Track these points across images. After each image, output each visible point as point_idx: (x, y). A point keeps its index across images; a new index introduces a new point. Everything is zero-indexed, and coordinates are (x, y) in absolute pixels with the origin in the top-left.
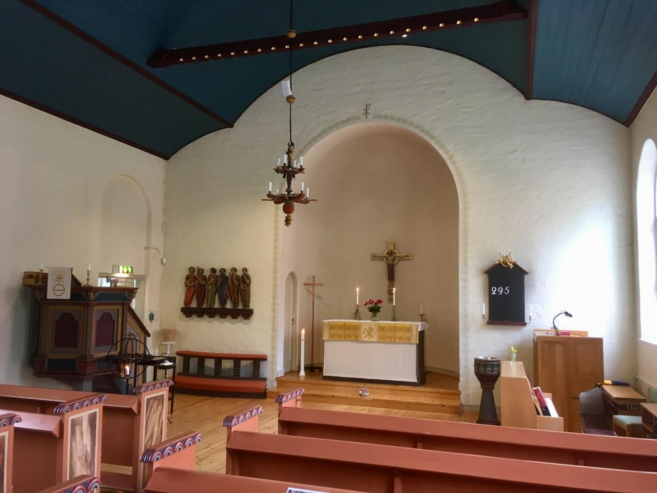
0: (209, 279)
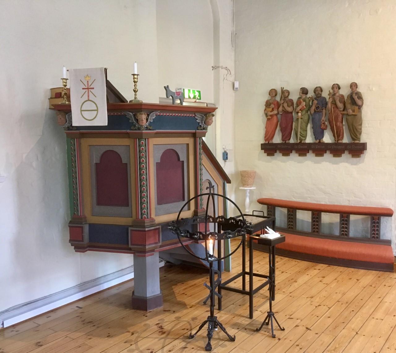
0: (299, 103)
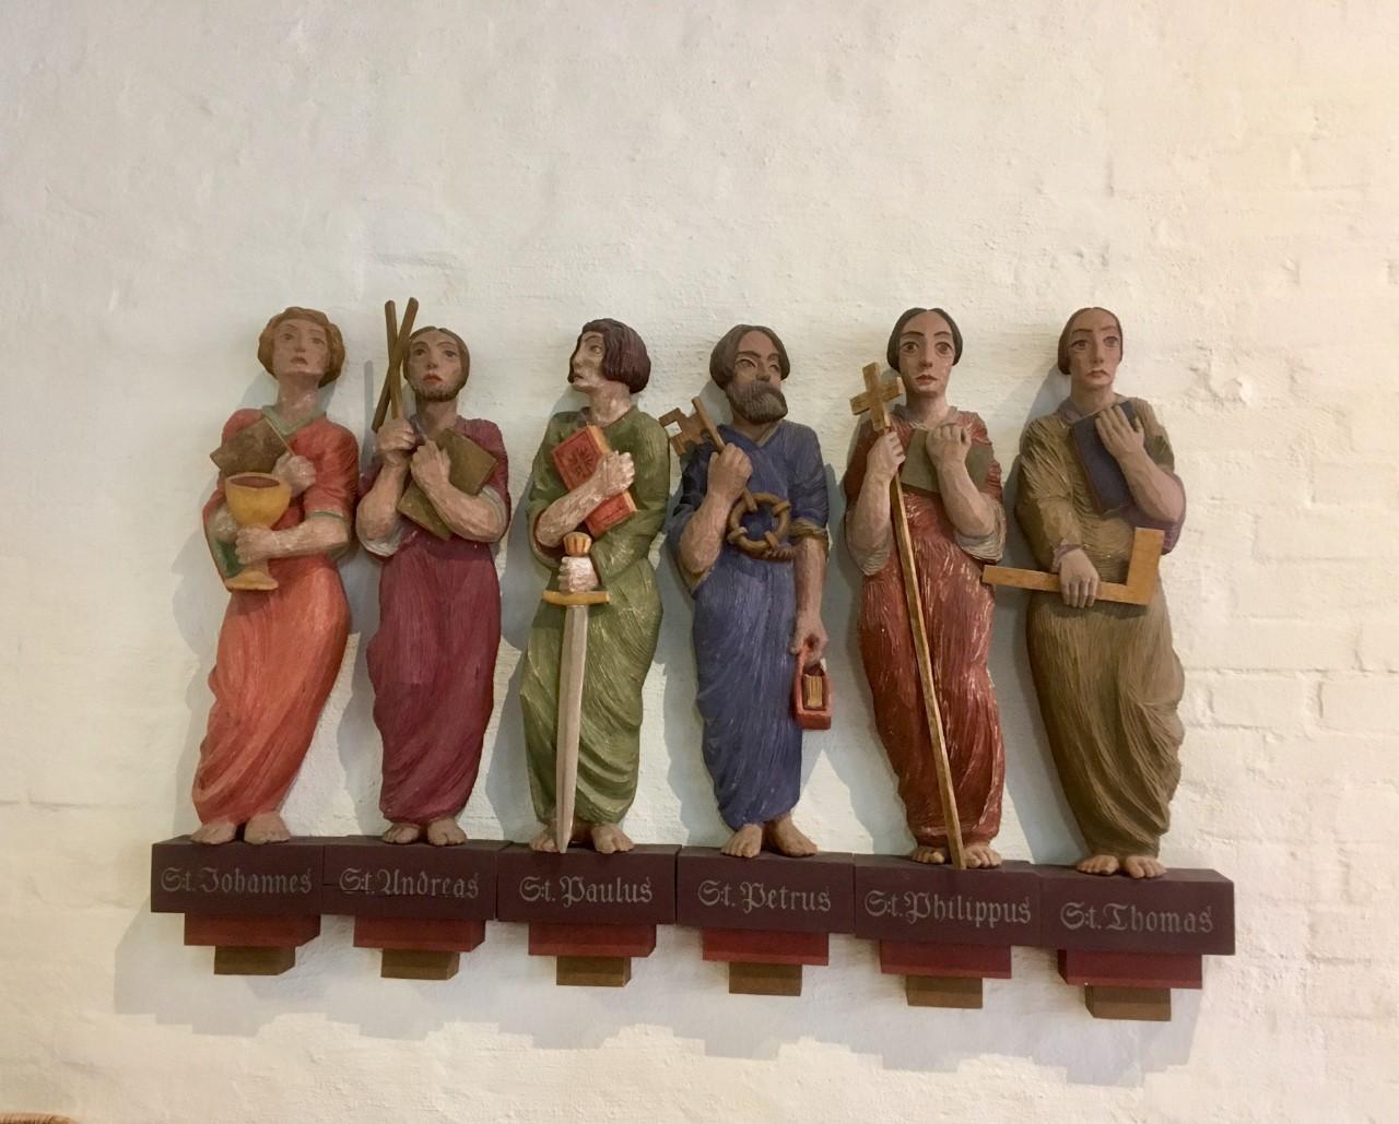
0: (564, 460)
